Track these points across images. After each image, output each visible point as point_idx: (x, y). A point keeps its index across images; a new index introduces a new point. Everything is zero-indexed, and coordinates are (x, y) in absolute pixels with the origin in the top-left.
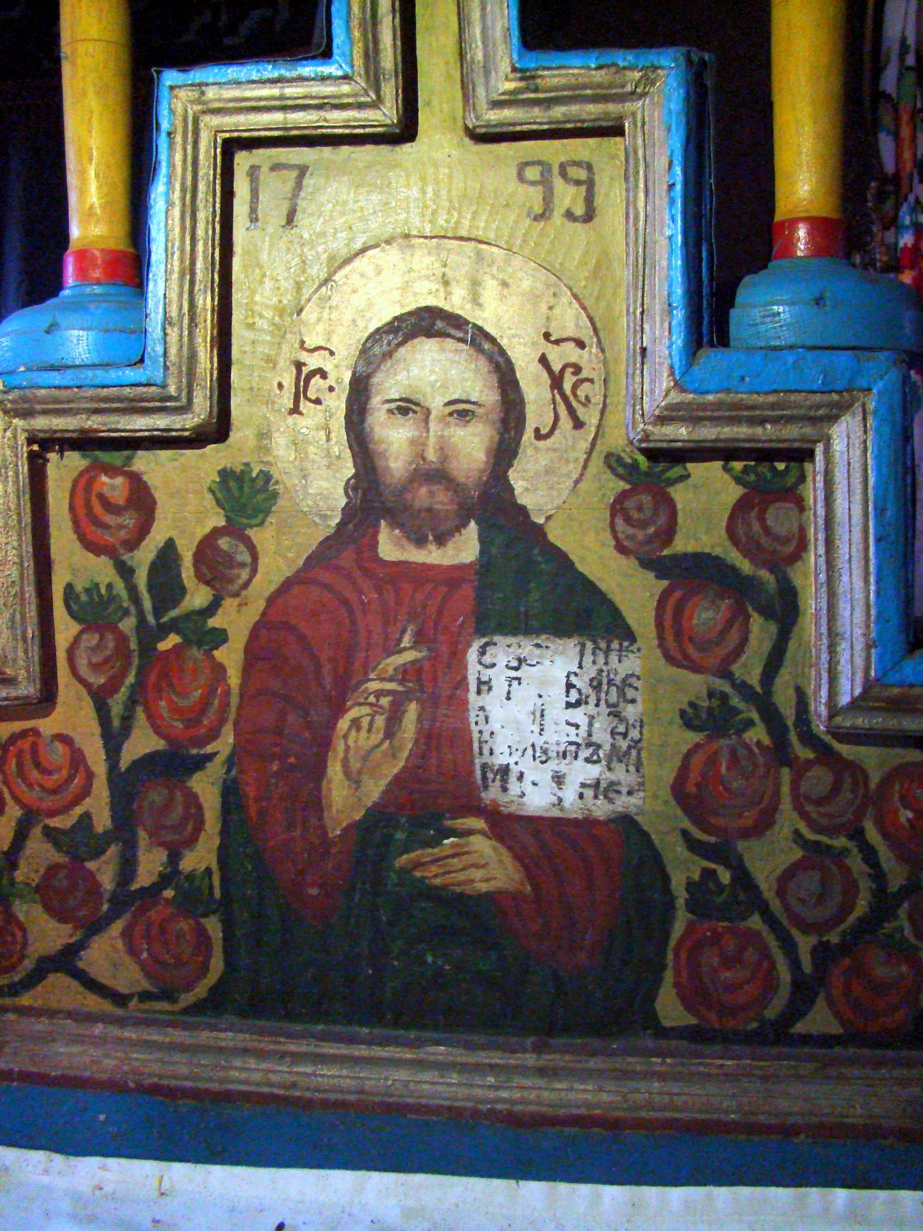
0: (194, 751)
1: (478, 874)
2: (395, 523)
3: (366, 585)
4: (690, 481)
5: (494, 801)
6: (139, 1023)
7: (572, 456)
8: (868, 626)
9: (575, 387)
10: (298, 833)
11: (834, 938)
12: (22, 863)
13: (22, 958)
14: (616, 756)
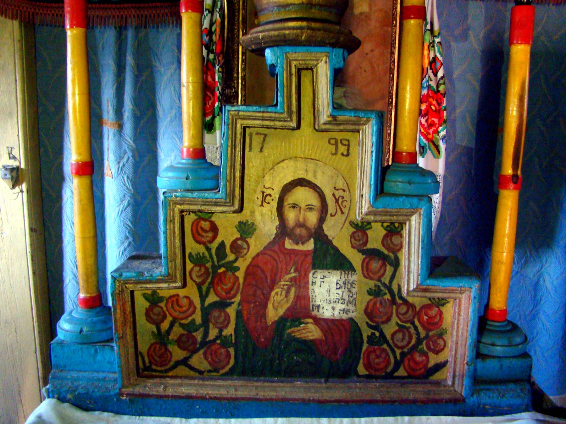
0: (228, 301)
1: (310, 334)
2: (290, 238)
3: (281, 255)
4: (372, 229)
5: (315, 315)
6: (208, 379)
7: (340, 221)
8: (418, 270)
9: (342, 202)
10: (259, 324)
11: (406, 350)
12: (172, 334)
13: (170, 361)
14: (349, 302)
